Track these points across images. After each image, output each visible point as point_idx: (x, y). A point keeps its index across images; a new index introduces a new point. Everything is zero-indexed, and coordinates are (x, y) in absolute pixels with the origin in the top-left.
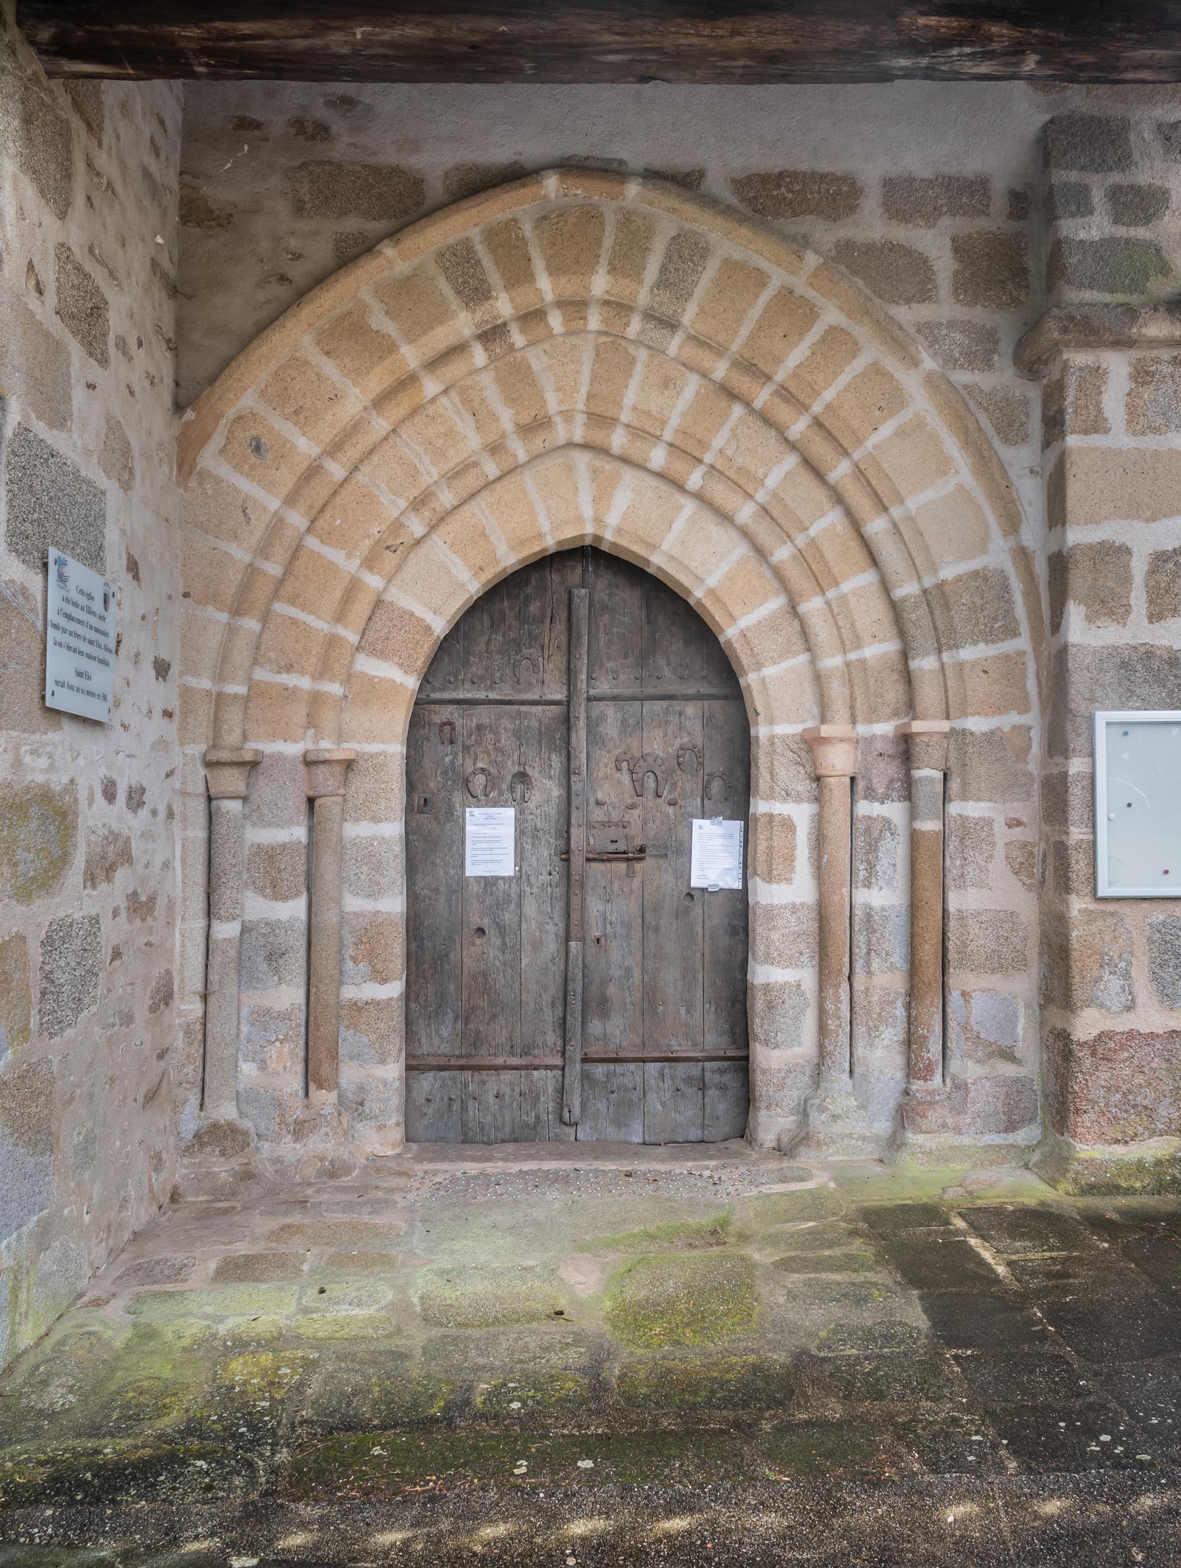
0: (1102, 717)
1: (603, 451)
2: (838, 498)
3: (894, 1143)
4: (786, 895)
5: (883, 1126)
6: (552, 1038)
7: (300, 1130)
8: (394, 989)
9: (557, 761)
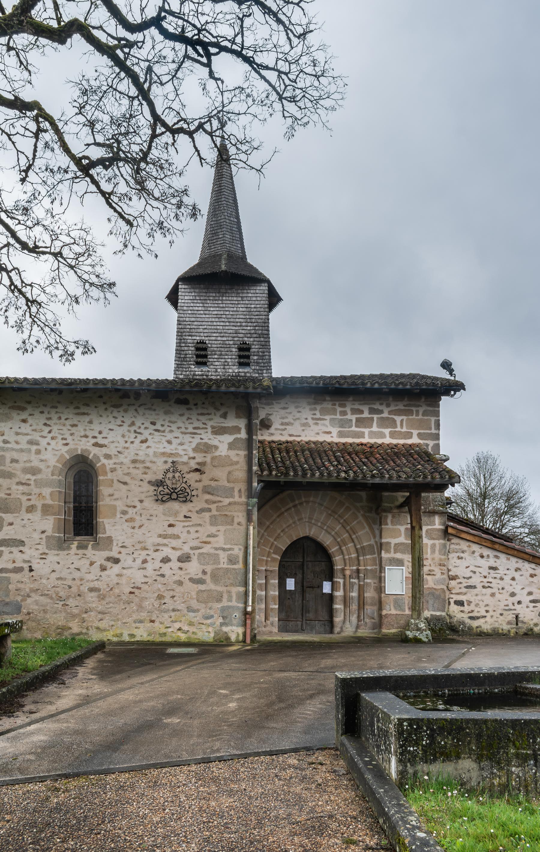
0: (387, 568)
1: (311, 523)
2: (348, 532)
3: (356, 631)
4: (339, 594)
5: (354, 630)
6: (300, 616)
7: (265, 627)
8: (277, 607)
9: (301, 571)
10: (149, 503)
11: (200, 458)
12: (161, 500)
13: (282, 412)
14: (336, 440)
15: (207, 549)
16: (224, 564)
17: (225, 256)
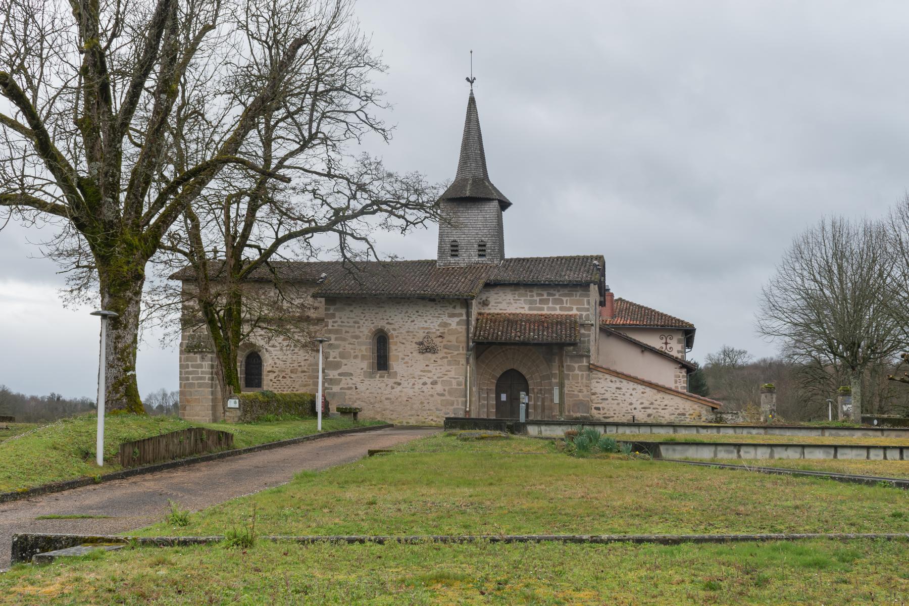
10: (416, 354)
11: (442, 330)
12: (421, 352)
13: (496, 296)
14: (528, 312)
15: (445, 378)
16: (454, 386)
17: (470, 182)
